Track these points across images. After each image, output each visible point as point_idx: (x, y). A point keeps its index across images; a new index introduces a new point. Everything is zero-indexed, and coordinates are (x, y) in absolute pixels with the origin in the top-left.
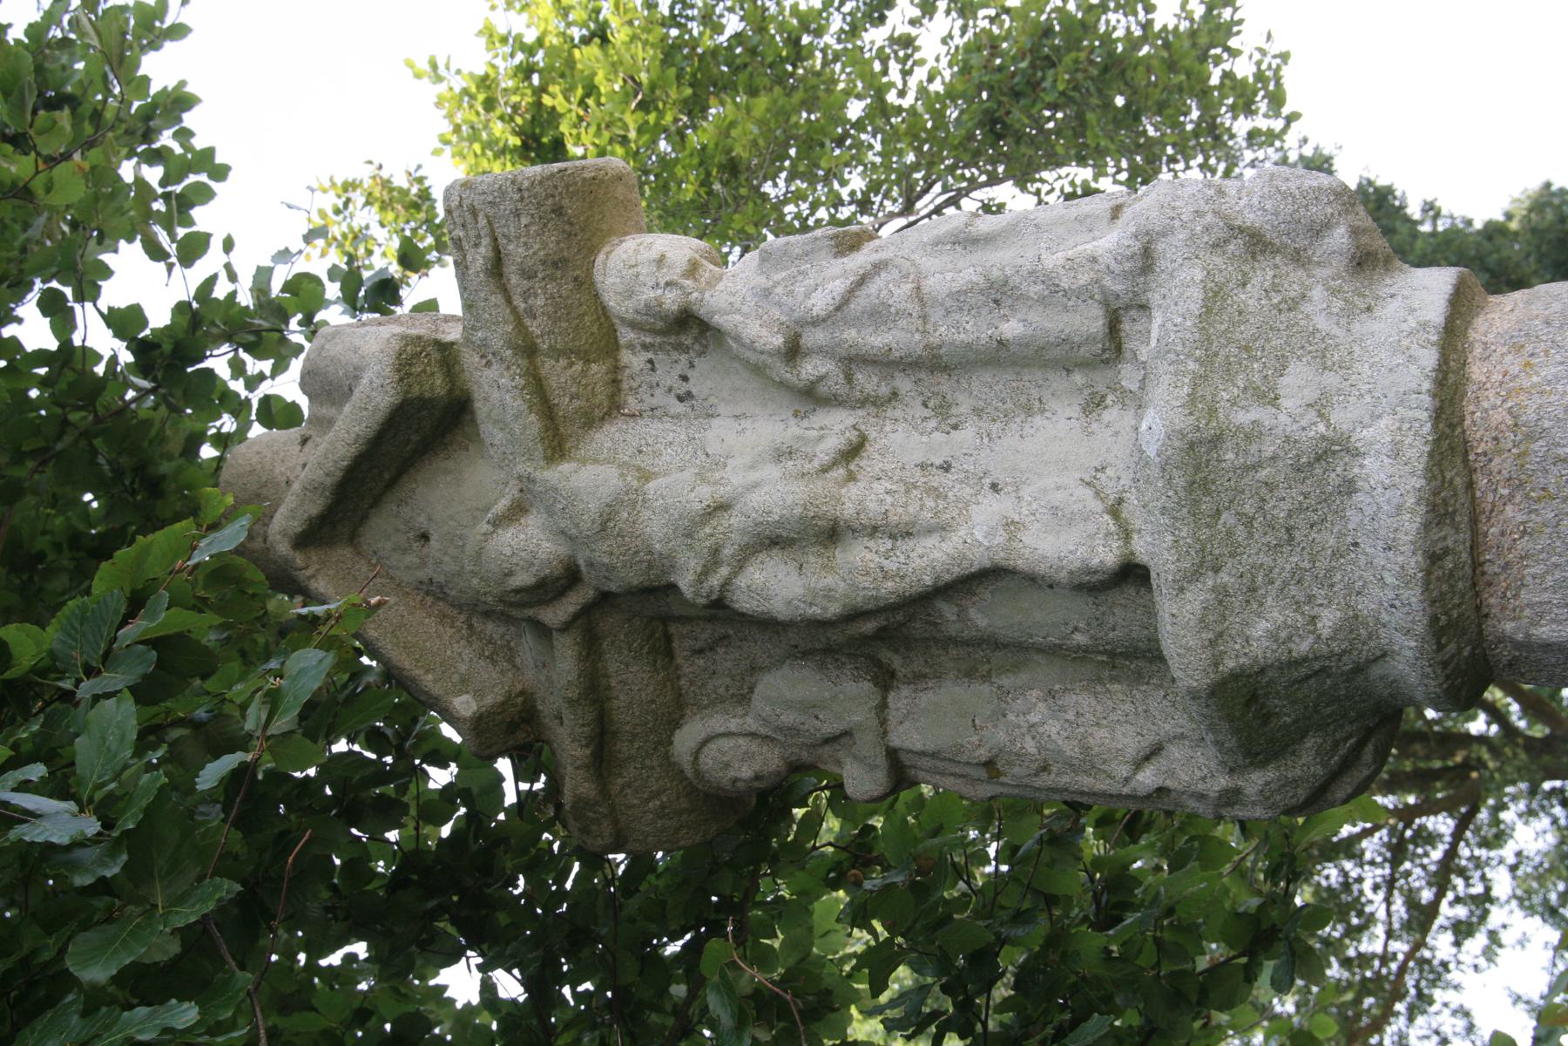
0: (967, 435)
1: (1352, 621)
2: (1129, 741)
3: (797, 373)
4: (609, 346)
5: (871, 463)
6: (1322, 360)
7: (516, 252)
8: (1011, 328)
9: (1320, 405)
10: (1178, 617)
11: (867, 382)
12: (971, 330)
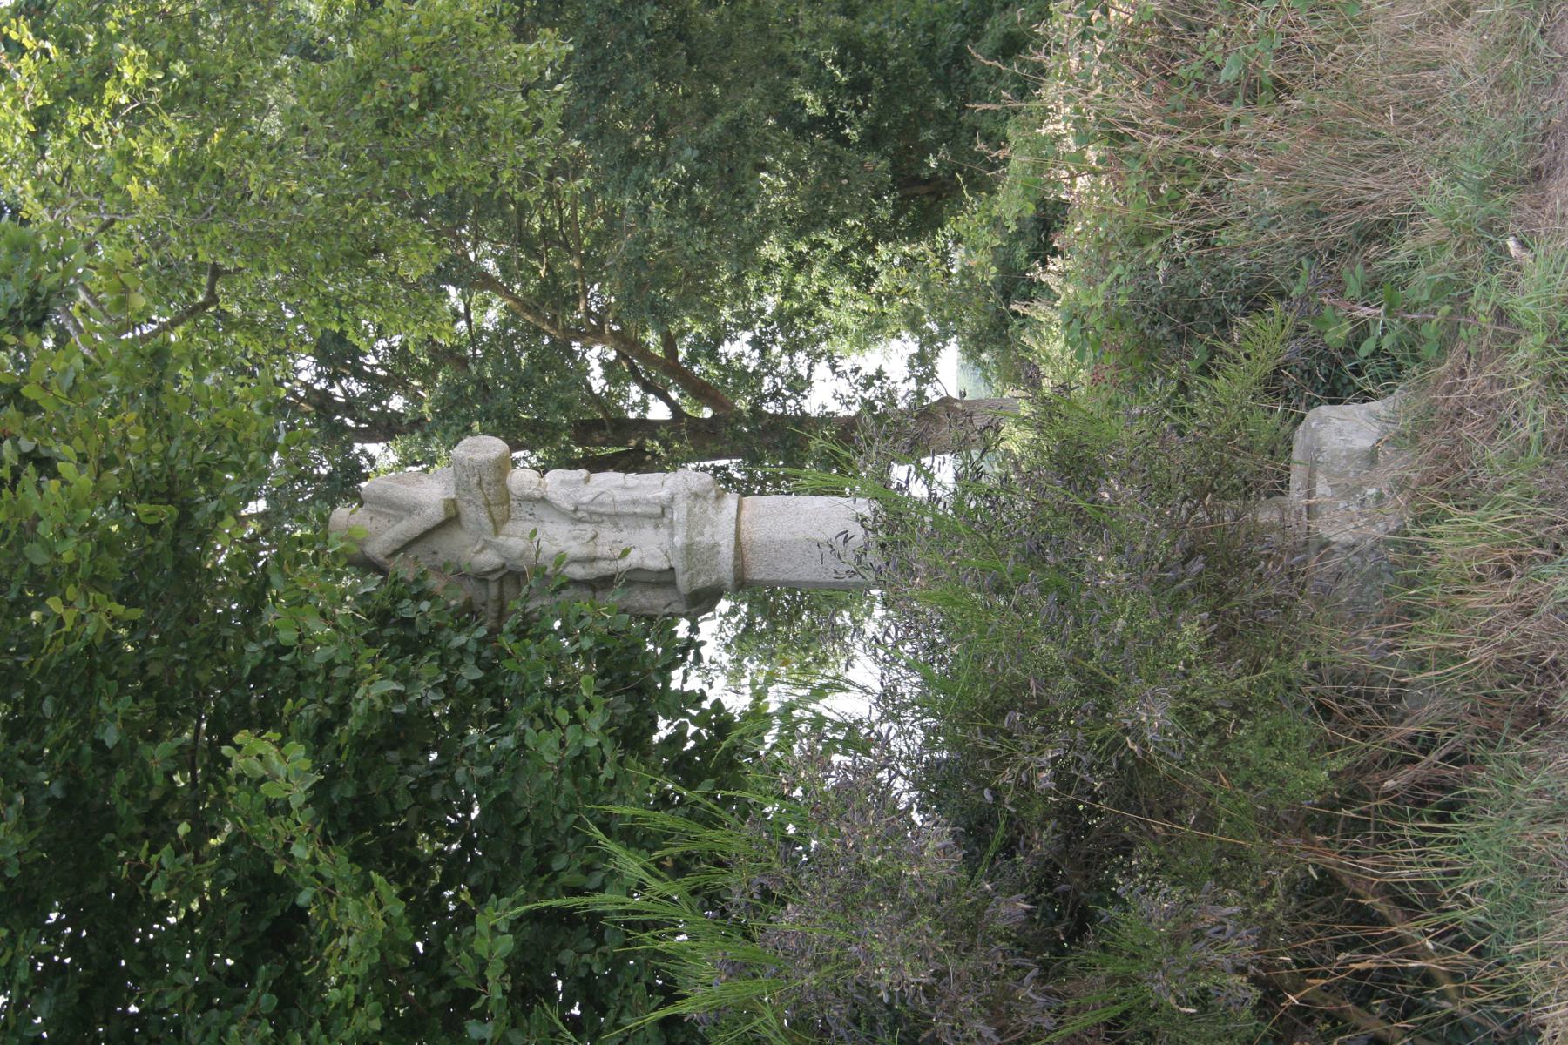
0: (625, 533)
1: (718, 579)
2: (663, 602)
3: (576, 516)
4: (507, 501)
5: (600, 540)
6: (712, 524)
7: (486, 478)
8: (638, 510)
9: (712, 536)
10: (682, 580)
11: (595, 518)
12: (627, 509)
